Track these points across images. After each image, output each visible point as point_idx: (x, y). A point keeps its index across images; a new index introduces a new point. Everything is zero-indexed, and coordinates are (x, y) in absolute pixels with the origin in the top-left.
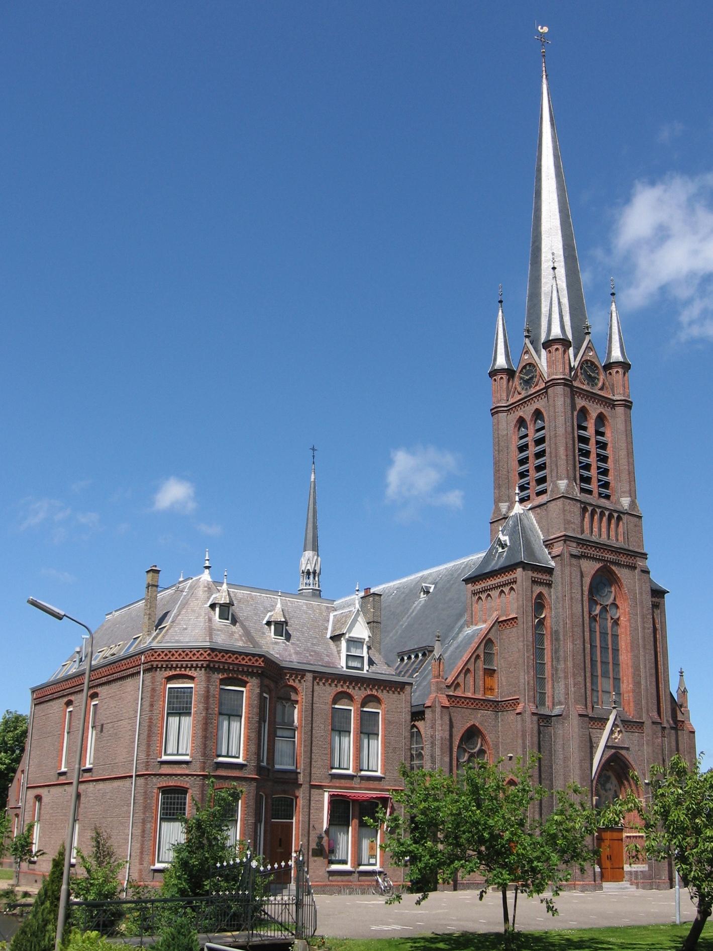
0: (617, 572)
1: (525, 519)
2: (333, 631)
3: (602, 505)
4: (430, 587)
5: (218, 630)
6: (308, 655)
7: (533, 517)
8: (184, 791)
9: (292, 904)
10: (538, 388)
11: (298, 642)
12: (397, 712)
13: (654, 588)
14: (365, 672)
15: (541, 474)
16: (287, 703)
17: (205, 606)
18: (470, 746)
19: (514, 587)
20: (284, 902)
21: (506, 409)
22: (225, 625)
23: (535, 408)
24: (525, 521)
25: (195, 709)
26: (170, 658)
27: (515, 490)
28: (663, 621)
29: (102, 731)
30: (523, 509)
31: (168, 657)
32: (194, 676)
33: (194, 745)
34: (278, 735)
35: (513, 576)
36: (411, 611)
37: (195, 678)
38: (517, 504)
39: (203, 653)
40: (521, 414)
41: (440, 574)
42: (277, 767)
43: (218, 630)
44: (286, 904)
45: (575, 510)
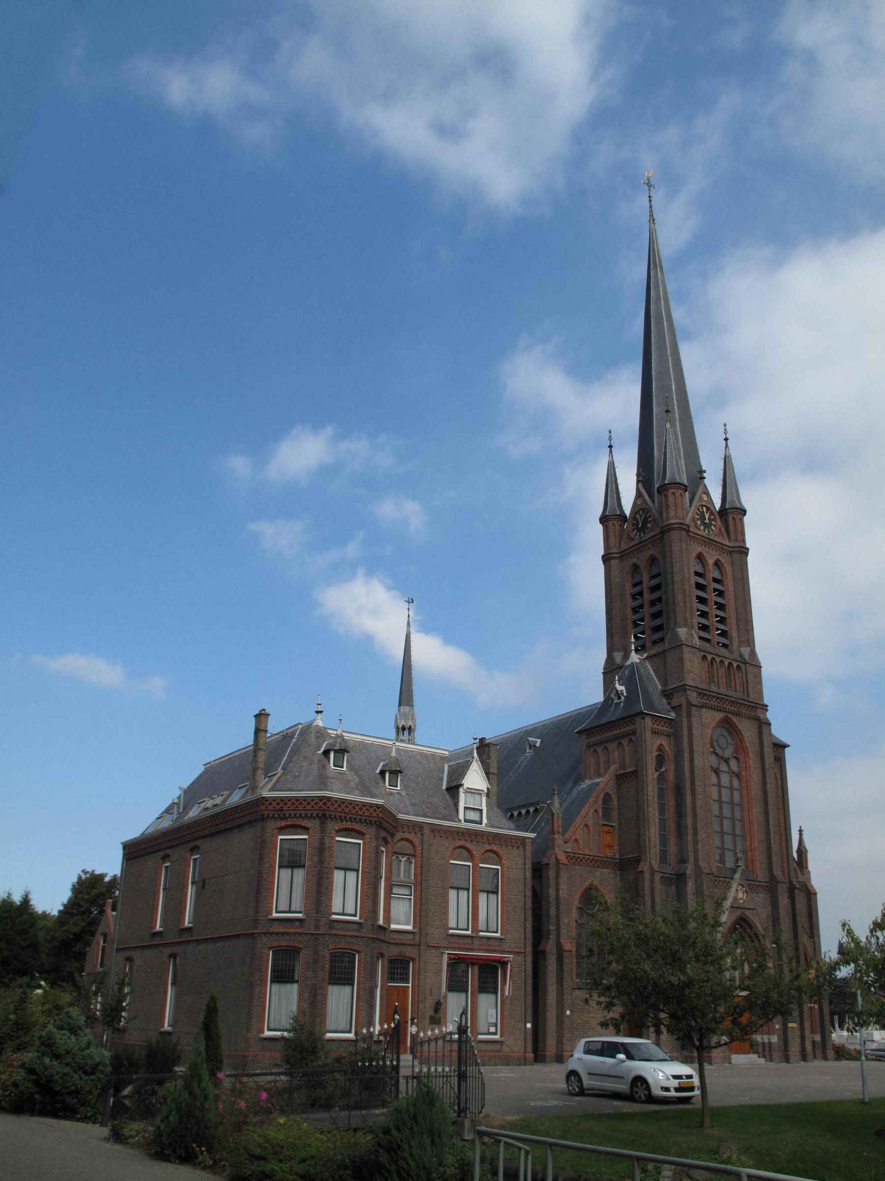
0: (738, 724)
1: (642, 669)
2: (448, 783)
3: (721, 654)
4: (537, 742)
5: (333, 778)
6: (424, 807)
7: (649, 666)
8: (296, 951)
9: (454, 1076)
10: (652, 534)
11: (413, 793)
12: (518, 869)
13: (775, 741)
14: (484, 825)
15: (657, 622)
16: (403, 857)
17: (319, 752)
18: (589, 906)
19: (633, 739)
20: (445, 1074)
21: (618, 555)
22: (339, 773)
23: (650, 553)
24: (642, 671)
25: (310, 863)
26: (282, 807)
27: (631, 638)
28: (784, 776)
29: (203, 887)
30: (639, 658)
31: (280, 806)
32: (309, 826)
33: (307, 901)
34: (394, 892)
35: (632, 727)
36: (517, 766)
37: (309, 828)
38: (633, 653)
39: (319, 802)
40: (635, 560)
41: (546, 728)
42: (394, 926)
43: (333, 778)
44: (447, 1076)
45: (695, 659)
